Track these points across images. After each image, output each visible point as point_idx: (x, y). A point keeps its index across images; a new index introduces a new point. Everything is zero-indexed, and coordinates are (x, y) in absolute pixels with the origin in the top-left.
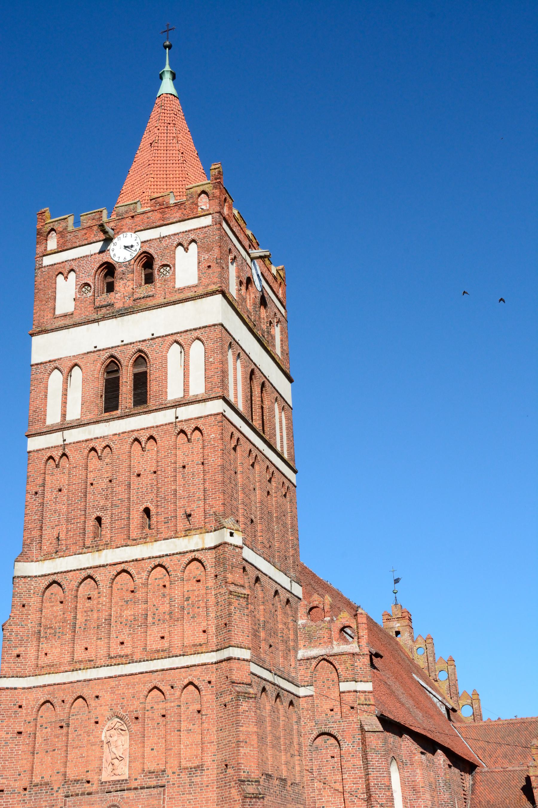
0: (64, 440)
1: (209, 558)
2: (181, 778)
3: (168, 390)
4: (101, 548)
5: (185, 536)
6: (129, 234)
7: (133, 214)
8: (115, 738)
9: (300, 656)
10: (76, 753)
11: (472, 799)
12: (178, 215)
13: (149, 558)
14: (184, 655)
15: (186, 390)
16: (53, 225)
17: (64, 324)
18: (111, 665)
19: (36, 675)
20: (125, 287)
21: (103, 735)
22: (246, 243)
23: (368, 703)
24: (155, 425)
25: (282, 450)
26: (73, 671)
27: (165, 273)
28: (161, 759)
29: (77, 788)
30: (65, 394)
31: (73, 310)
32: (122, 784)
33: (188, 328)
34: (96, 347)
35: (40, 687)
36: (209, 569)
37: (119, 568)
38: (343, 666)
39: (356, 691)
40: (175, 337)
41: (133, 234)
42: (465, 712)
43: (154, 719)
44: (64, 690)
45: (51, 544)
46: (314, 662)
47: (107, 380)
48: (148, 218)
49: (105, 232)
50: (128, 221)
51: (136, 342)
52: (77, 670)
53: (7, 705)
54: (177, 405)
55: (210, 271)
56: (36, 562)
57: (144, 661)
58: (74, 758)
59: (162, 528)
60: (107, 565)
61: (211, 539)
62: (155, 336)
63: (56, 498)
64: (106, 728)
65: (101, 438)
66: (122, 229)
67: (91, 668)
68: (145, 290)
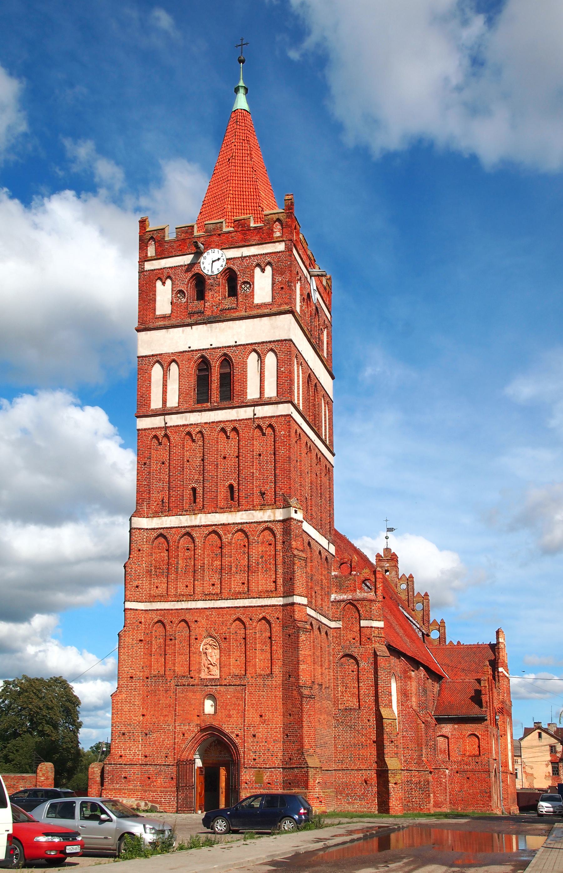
0: (166, 423)
1: (278, 529)
3: (248, 391)
4: (196, 512)
5: (260, 510)
6: (216, 250)
8: (210, 651)
9: (332, 599)
11: (438, 700)
12: (257, 238)
13: (234, 524)
14: (259, 598)
15: (164, 401)
16: (153, 234)
17: (164, 325)
18: (206, 600)
20: (216, 296)
22: (307, 263)
23: (380, 636)
24: (238, 419)
25: (299, 403)
26: (178, 601)
27: (246, 288)
29: (184, 681)
30: (165, 386)
31: (170, 312)
34: (190, 347)
35: (154, 610)
36: (278, 536)
37: (211, 529)
38: (364, 609)
39: (372, 627)
40: (254, 347)
42: (435, 635)
44: (172, 614)
45: (158, 504)
46: (343, 604)
47: (198, 376)
48: (232, 237)
49: (197, 247)
50: (215, 239)
51: (223, 347)
52: (181, 601)
54: (255, 404)
55: (283, 292)
56: (147, 518)
57: (230, 599)
59: (243, 501)
60: (201, 526)
61: (279, 515)
64: (203, 643)
65: (195, 424)
66: (210, 245)
68: (229, 302)
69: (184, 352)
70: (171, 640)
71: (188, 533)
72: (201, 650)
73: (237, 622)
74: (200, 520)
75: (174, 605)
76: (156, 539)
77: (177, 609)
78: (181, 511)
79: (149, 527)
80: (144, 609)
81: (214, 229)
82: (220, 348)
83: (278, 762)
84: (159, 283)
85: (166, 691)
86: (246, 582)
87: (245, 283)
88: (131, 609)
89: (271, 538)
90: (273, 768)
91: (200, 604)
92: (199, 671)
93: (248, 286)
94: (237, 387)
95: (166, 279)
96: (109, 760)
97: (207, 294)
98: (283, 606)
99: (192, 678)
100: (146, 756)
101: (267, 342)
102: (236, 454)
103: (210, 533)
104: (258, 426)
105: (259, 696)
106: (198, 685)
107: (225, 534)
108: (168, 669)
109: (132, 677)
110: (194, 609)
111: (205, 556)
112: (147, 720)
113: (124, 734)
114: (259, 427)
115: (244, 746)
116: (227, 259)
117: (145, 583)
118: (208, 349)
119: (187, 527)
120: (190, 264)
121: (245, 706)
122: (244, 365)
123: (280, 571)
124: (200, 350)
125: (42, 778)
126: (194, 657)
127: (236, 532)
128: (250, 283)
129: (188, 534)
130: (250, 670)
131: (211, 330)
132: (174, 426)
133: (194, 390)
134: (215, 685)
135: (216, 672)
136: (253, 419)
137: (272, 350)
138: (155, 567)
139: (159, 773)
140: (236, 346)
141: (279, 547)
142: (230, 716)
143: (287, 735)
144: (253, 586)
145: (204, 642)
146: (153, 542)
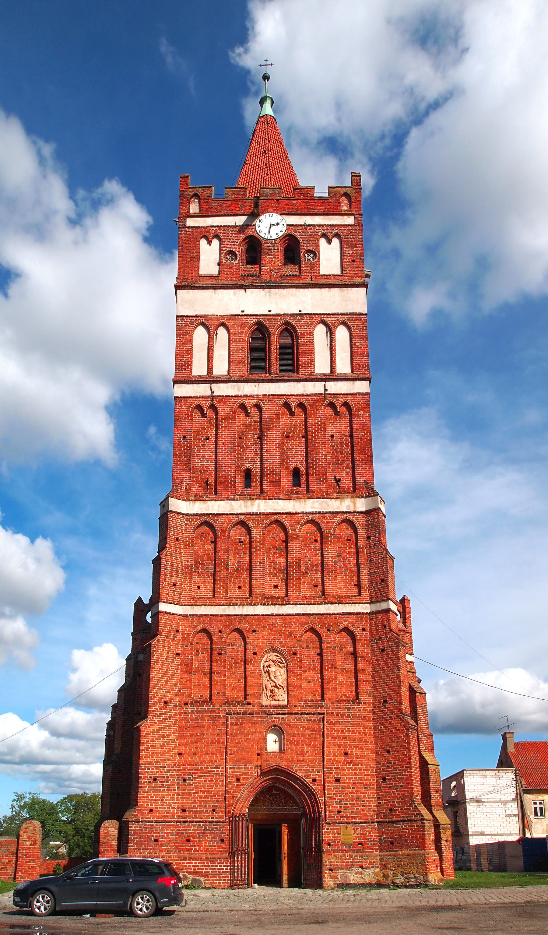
1: (360, 523)
2: (340, 708)
5: (337, 498)
6: (275, 215)
7: (279, 198)
10: (234, 678)
13: (303, 513)
14: (339, 604)
15: (210, 367)
18: (268, 605)
19: (191, 605)
20: (272, 262)
21: (262, 665)
26: (230, 605)
28: (318, 691)
32: (283, 708)
33: (336, 312)
34: (243, 311)
35: (196, 615)
37: (272, 518)
40: (322, 317)
41: (279, 216)
43: (310, 657)
44: (221, 621)
45: (200, 486)
48: (293, 204)
51: (284, 314)
52: (233, 605)
53: (167, 627)
54: (325, 379)
57: (300, 604)
58: (232, 682)
60: (260, 513)
62: (302, 312)
63: (203, 445)
64: (264, 659)
65: (250, 396)
66: (268, 209)
67: (247, 605)
69: (236, 315)
70: (220, 654)
71: (242, 522)
72: (262, 668)
73: (309, 634)
74: (259, 506)
75: (224, 610)
76: (198, 527)
77: (228, 615)
78: (231, 496)
79: (190, 512)
80: (182, 614)
81: (271, 194)
82: (281, 315)
83: (371, 815)
84: (203, 242)
85: (213, 721)
86: (320, 584)
87: (309, 251)
88: (166, 613)
89: (351, 533)
90: (366, 823)
91: (260, 610)
92: (260, 697)
93: (312, 255)
94: (303, 359)
95: (213, 238)
96: (136, 816)
97: (263, 257)
98: (370, 613)
99: (249, 704)
100: (184, 811)
101: (338, 314)
102: (303, 433)
103: (271, 523)
104: (332, 404)
105: (342, 728)
106: (259, 714)
107: (291, 525)
108: (215, 692)
109: (166, 703)
110: (252, 615)
111: (265, 550)
112: (186, 761)
113: (155, 779)
114: (332, 405)
115: (325, 793)
116: (287, 225)
117: (184, 581)
118: (266, 315)
119: (241, 514)
120: (243, 225)
121: (324, 741)
122: (311, 334)
123: (364, 571)
124: (257, 315)
125: (27, 843)
126: (252, 677)
127: (306, 523)
128: (315, 253)
129: (243, 523)
130: (328, 694)
131: (270, 295)
132: (223, 396)
133: (248, 358)
134: (282, 714)
135: (282, 697)
136: (325, 395)
137: (344, 323)
138: (197, 562)
139: (203, 834)
140: (300, 315)
141: (362, 542)
142: (303, 755)
143: (384, 779)
144: (330, 589)
145: (265, 658)
146: (194, 531)
